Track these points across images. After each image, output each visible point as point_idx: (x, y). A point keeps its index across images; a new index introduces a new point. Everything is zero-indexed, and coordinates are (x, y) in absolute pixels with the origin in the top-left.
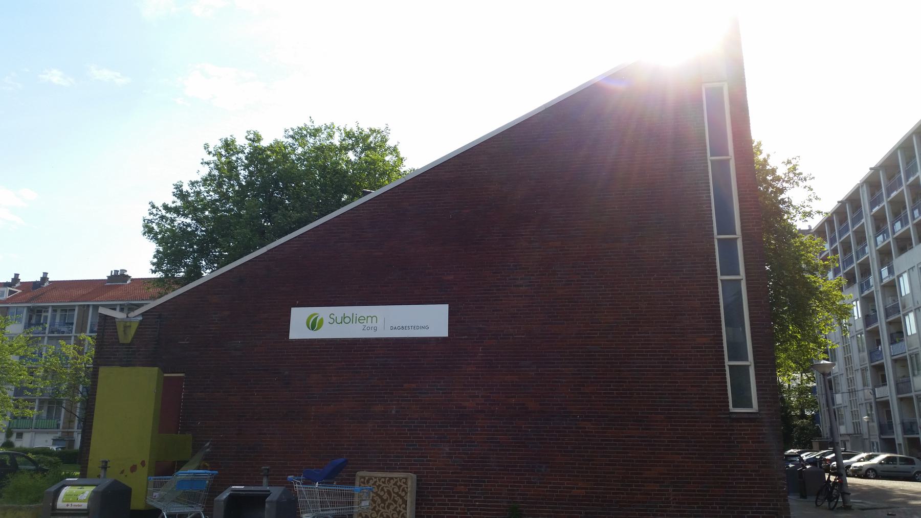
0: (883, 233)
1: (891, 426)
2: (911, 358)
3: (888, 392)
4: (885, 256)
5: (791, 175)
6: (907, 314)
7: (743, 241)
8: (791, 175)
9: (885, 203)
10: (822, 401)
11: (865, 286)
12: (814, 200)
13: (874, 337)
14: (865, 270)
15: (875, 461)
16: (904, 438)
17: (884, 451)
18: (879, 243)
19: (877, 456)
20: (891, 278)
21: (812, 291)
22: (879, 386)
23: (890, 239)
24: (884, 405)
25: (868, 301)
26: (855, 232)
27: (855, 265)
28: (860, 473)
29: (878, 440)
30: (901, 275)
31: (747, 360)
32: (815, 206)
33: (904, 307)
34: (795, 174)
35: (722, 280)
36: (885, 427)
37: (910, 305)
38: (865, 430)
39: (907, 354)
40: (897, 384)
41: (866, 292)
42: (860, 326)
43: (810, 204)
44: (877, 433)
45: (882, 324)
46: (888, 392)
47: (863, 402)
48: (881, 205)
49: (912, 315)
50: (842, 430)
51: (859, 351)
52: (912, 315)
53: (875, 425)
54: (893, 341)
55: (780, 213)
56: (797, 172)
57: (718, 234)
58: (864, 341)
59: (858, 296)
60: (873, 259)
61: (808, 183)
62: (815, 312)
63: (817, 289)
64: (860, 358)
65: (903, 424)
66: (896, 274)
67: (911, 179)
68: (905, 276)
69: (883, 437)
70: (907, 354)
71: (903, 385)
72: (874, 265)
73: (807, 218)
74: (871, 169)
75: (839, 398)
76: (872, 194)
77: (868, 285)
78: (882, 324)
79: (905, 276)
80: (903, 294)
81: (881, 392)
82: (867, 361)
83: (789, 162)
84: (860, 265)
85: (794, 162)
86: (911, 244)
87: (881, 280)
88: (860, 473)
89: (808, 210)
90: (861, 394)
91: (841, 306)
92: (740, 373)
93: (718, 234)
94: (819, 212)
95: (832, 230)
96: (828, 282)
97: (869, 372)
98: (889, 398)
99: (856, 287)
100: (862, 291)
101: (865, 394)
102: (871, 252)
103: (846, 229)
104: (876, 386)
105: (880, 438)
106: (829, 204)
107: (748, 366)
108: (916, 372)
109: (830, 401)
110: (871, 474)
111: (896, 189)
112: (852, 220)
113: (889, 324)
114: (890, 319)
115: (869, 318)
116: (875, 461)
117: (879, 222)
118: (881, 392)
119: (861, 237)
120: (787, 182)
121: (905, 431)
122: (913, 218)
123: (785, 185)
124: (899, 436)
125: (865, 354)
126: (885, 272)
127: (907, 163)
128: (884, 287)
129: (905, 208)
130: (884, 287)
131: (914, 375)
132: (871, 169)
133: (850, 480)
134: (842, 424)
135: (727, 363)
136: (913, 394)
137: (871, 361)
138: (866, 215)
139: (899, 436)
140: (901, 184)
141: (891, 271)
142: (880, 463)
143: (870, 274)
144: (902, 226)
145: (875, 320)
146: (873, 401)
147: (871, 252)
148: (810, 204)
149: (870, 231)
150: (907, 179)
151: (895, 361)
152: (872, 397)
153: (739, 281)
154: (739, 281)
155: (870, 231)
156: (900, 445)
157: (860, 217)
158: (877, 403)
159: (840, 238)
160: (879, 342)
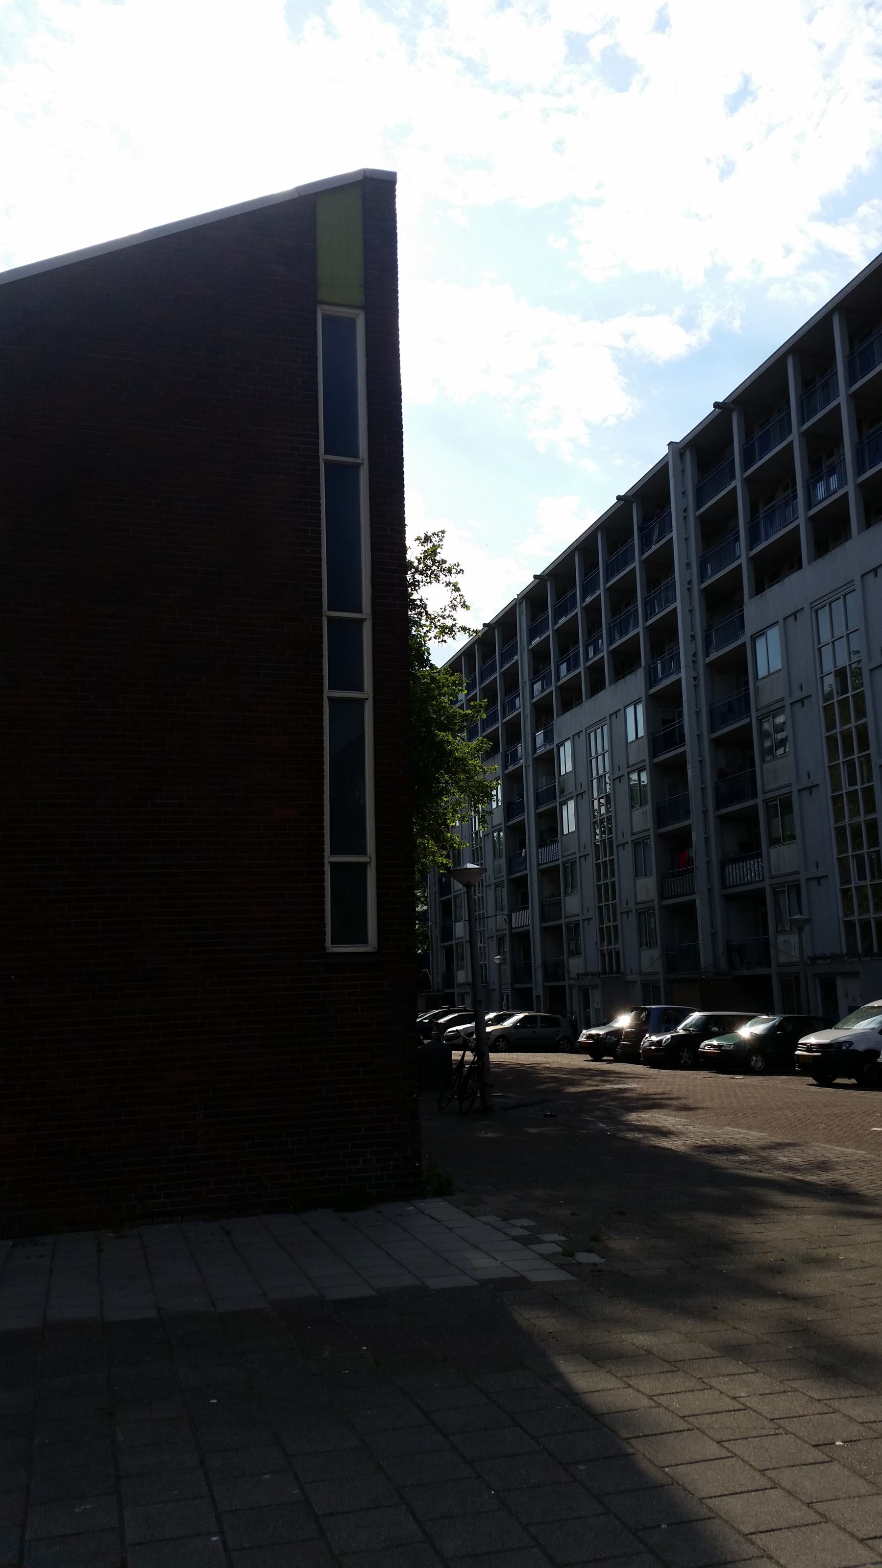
0: (542, 679)
1: (528, 969)
2: (565, 868)
3: (528, 919)
4: (543, 714)
5: (429, 562)
6: (565, 803)
7: (374, 625)
8: (429, 562)
9: (550, 632)
10: (435, 933)
11: (510, 758)
12: (459, 608)
13: (516, 834)
14: (513, 732)
15: (508, 1023)
16: (544, 987)
17: (521, 1009)
18: (562, 675)
19: (511, 1016)
20: (548, 747)
21: (443, 758)
22: (517, 910)
23: (553, 688)
24: (521, 938)
25: (513, 781)
26: (504, 674)
27: (499, 724)
28: (509, 1041)
29: (509, 991)
30: (562, 744)
31: (363, 852)
32: (462, 618)
33: (562, 791)
34: (434, 561)
35: (331, 699)
36: (521, 971)
37: (570, 787)
38: (493, 976)
39: (560, 862)
40: (542, 907)
41: (511, 768)
42: (498, 818)
43: (453, 613)
44: (509, 981)
45: (529, 816)
46: (528, 919)
47: (494, 933)
48: (546, 635)
49: (571, 804)
50: (575, 965)
51: (494, 857)
52: (571, 804)
53: (507, 968)
54: (542, 843)
55: (410, 623)
56: (438, 558)
57: (330, 609)
58: (502, 841)
59: (499, 772)
60: (525, 717)
61: (453, 578)
62: (445, 791)
63: (451, 752)
64: (495, 867)
65: (545, 965)
66: (556, 741)
67: (589, 599)
68: (568, 744)
69: (547, 984)
70: (560, 862)
71: (551, 908)
72: (527, 726)
73: (446, 637)
74: (535, 577)
75: (571, 904)
76: (559, 595)
77: (515, 759)
78: (529, 816)
79: (568, 744)
80: (563, 773)
81: (521, 919)
82: (504, 872)
83: (427, 539)
84: (506, 725)
85: (435, 540)
86: (580, 698)
87: (535, 749)
88: (509, 1041)
89: (449, 622)
90: (491, 923)
91: (481, 782)
92: (349, 879)
93: (330, 609)
94: (464, 629)
95: (471, 670)
96: (462, 746)
97: (505, 890)
98: (530, 928)
99: (499, 757)
100: (505, 766)
101: (495, 922)
102: (523, 707)
103: (493, 669)
104: (513, 909)
105: (512, 988)
106: (481, 613)
107: (364, 866)
108: (569, 890)
109: (447, 933)
110: (501, 1044)
111: (565, 614)
112: (502, 655)
113: (539, 816)
114: (540, 810)
115: (512, 807)
116: (508, 1023)
117: (539, 657)
118: (521, 919)
119: (511, 681)
120: (421, 573)
121: (547, 977)
122: (587, 659)
123: (418, 577)
124: (538, 985)
125: (503, 862)
126: (540, 736)
127: (586, 574)
128: (538, 760)
129: (576, 642)
130: (538, 760)
131: (566, 894)
132: (535, 577)
133: (494, 1057)
134: (576, 952)
135: (329, 858)
136: (563, 921)
137: (510, 871)
138: (522, 649)
139: (538, 985)
140: (574, 606)
141: (548, 738)
142: (515, 1026)
143: (519, 740)
144: (569, 670)
145: (520, 809)
146: (507, 932)
147: (523, 707)
148: (453, 613)
149: (525, 673)
150: (583, 599)
151: (542, 872)
152: (506, 926)
153: (362, 701)
154: (362, 701)
155: (525, 673)
156: (538, 997)
157: (513, 651)
158: (512, 935)
159: (481, 682)
160: (523, 844)
